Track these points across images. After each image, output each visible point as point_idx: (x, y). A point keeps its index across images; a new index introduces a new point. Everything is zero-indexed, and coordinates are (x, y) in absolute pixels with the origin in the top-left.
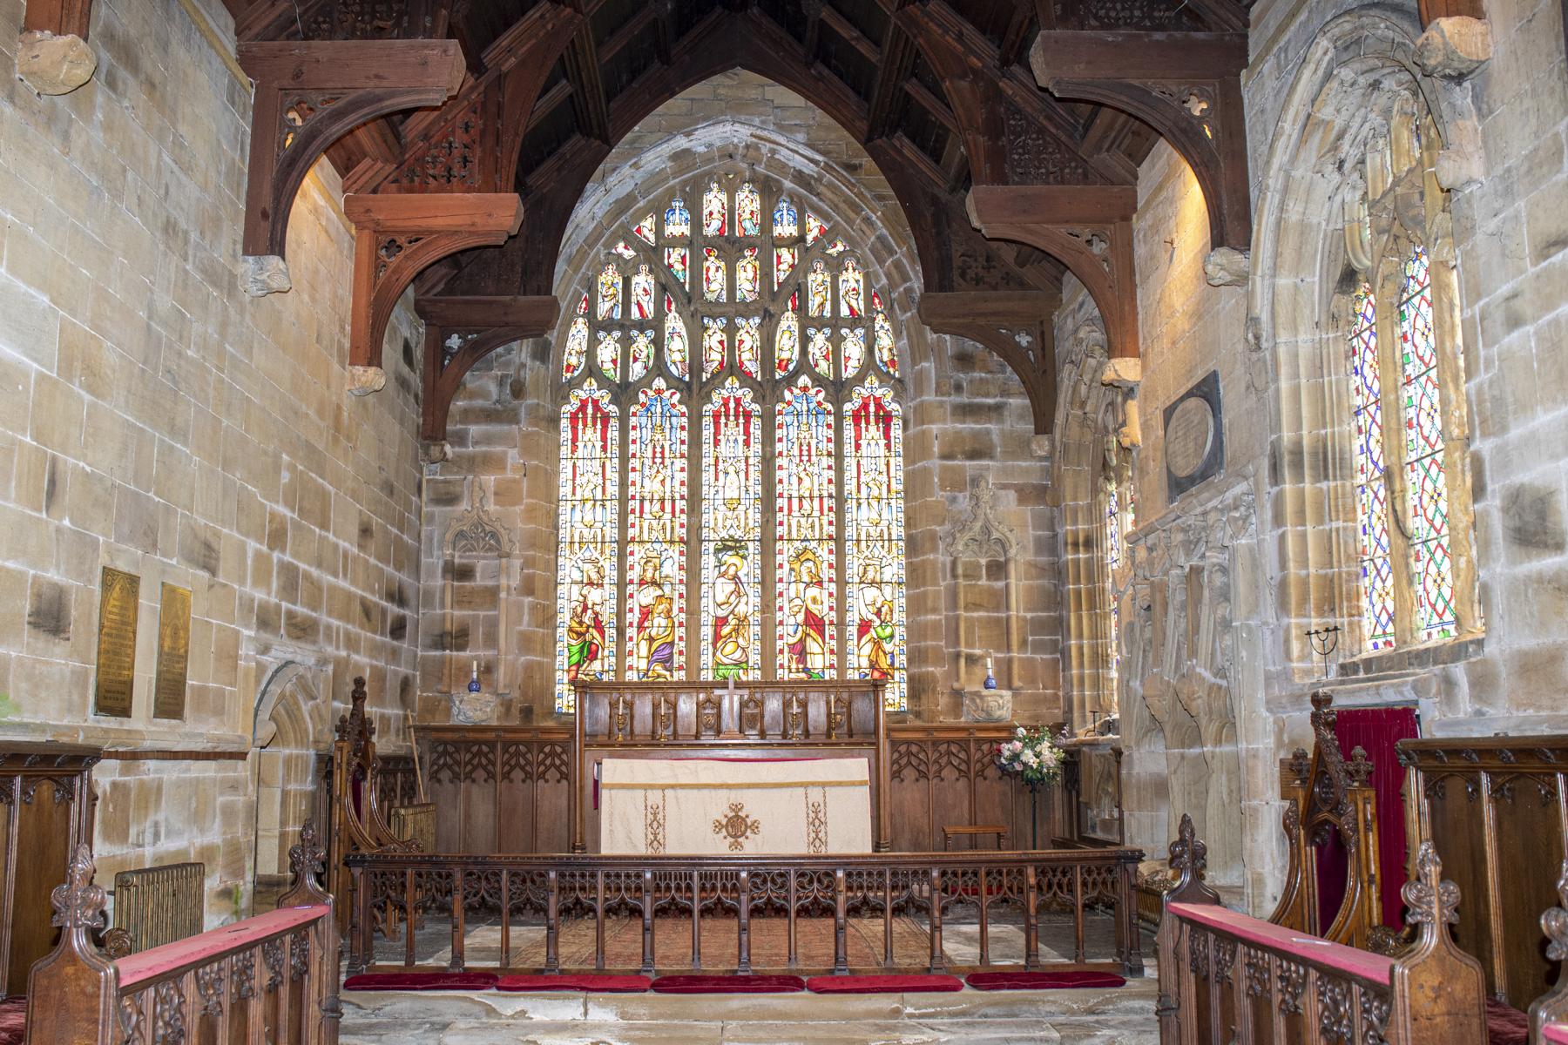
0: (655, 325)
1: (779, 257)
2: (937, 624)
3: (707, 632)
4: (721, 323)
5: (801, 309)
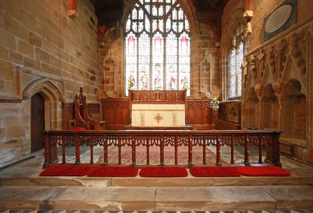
0: (143, 21)
1: (167, 7)
2: (196, 80)
3: (153, 82)
4: (156, 21)
5: (171, 18)
